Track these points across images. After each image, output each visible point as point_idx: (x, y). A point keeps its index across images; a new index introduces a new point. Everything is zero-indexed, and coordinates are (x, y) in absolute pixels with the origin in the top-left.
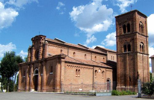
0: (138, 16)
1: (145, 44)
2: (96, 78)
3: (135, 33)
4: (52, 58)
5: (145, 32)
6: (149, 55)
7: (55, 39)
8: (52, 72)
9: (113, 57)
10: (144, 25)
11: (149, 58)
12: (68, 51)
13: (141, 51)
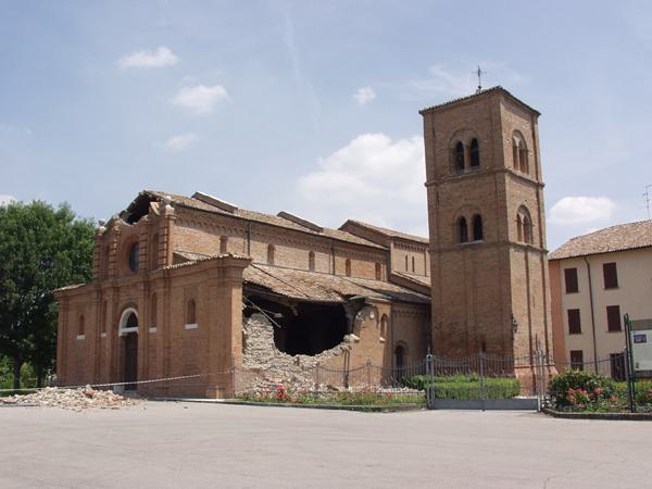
0: (511, 120)
1: (534, 214)
2: (356, 341)
3: (498, 171)
4: (193, 270)
5: (532, 167)
6: (543, 186)
7: (279, 215)
8: (193, 322)
9: (410, 260)
10: (530, 146)
11: (223, 248)
12: (526, 258)
13: (519, 240)
